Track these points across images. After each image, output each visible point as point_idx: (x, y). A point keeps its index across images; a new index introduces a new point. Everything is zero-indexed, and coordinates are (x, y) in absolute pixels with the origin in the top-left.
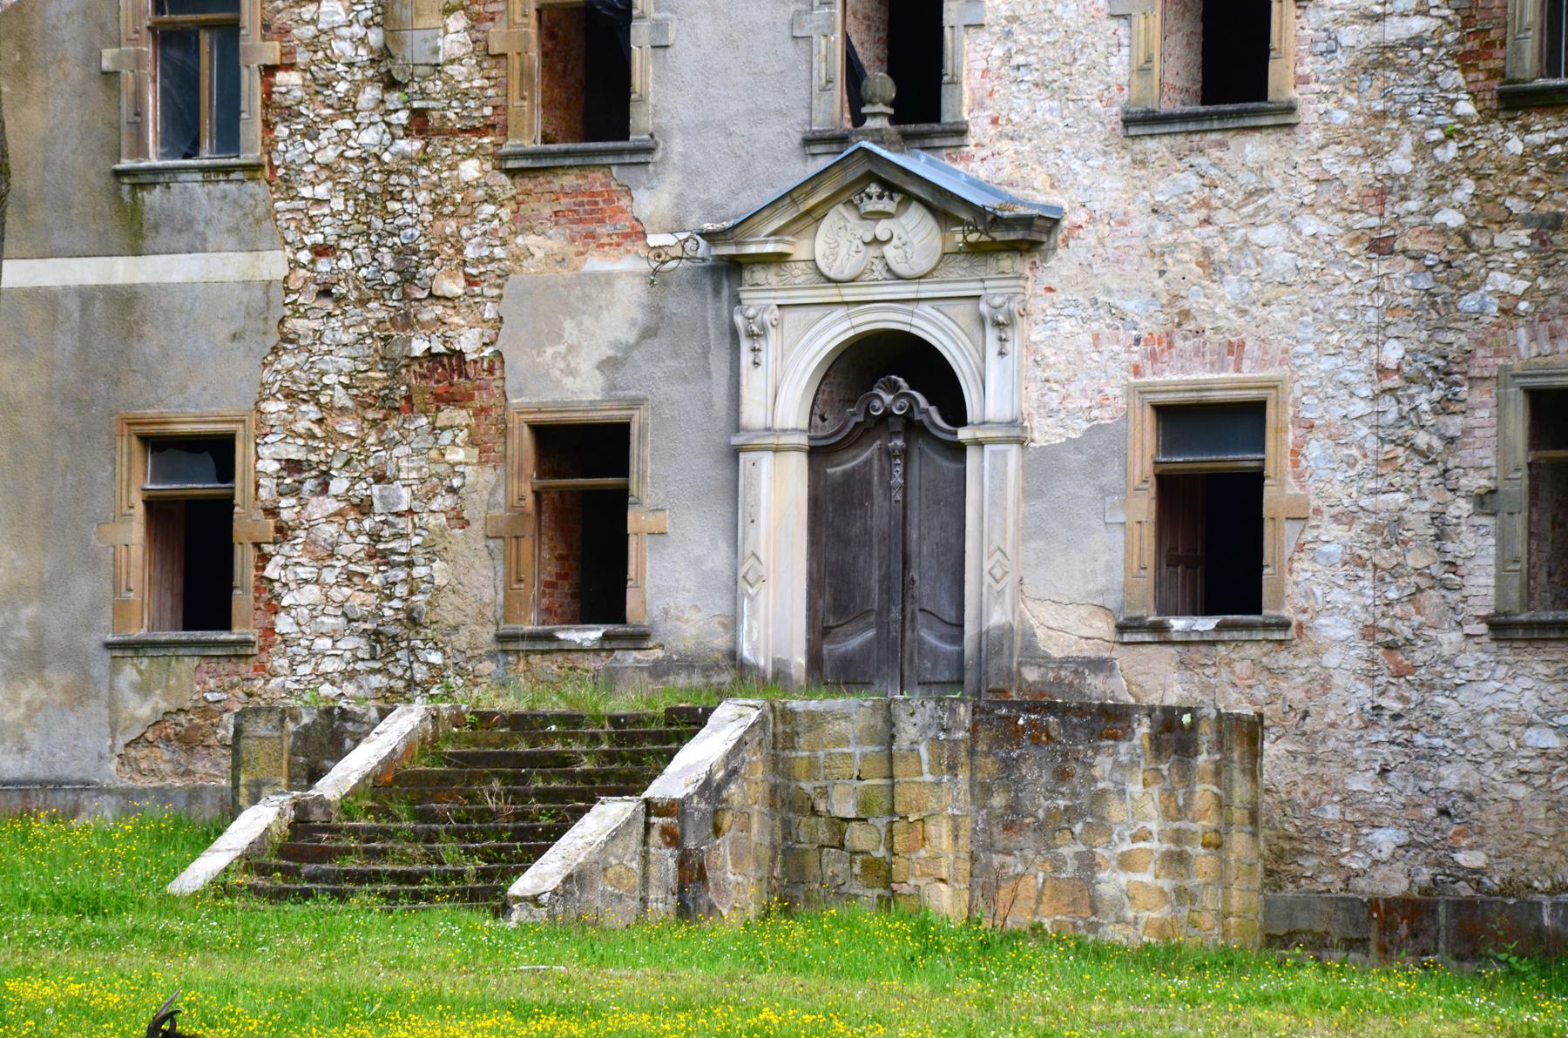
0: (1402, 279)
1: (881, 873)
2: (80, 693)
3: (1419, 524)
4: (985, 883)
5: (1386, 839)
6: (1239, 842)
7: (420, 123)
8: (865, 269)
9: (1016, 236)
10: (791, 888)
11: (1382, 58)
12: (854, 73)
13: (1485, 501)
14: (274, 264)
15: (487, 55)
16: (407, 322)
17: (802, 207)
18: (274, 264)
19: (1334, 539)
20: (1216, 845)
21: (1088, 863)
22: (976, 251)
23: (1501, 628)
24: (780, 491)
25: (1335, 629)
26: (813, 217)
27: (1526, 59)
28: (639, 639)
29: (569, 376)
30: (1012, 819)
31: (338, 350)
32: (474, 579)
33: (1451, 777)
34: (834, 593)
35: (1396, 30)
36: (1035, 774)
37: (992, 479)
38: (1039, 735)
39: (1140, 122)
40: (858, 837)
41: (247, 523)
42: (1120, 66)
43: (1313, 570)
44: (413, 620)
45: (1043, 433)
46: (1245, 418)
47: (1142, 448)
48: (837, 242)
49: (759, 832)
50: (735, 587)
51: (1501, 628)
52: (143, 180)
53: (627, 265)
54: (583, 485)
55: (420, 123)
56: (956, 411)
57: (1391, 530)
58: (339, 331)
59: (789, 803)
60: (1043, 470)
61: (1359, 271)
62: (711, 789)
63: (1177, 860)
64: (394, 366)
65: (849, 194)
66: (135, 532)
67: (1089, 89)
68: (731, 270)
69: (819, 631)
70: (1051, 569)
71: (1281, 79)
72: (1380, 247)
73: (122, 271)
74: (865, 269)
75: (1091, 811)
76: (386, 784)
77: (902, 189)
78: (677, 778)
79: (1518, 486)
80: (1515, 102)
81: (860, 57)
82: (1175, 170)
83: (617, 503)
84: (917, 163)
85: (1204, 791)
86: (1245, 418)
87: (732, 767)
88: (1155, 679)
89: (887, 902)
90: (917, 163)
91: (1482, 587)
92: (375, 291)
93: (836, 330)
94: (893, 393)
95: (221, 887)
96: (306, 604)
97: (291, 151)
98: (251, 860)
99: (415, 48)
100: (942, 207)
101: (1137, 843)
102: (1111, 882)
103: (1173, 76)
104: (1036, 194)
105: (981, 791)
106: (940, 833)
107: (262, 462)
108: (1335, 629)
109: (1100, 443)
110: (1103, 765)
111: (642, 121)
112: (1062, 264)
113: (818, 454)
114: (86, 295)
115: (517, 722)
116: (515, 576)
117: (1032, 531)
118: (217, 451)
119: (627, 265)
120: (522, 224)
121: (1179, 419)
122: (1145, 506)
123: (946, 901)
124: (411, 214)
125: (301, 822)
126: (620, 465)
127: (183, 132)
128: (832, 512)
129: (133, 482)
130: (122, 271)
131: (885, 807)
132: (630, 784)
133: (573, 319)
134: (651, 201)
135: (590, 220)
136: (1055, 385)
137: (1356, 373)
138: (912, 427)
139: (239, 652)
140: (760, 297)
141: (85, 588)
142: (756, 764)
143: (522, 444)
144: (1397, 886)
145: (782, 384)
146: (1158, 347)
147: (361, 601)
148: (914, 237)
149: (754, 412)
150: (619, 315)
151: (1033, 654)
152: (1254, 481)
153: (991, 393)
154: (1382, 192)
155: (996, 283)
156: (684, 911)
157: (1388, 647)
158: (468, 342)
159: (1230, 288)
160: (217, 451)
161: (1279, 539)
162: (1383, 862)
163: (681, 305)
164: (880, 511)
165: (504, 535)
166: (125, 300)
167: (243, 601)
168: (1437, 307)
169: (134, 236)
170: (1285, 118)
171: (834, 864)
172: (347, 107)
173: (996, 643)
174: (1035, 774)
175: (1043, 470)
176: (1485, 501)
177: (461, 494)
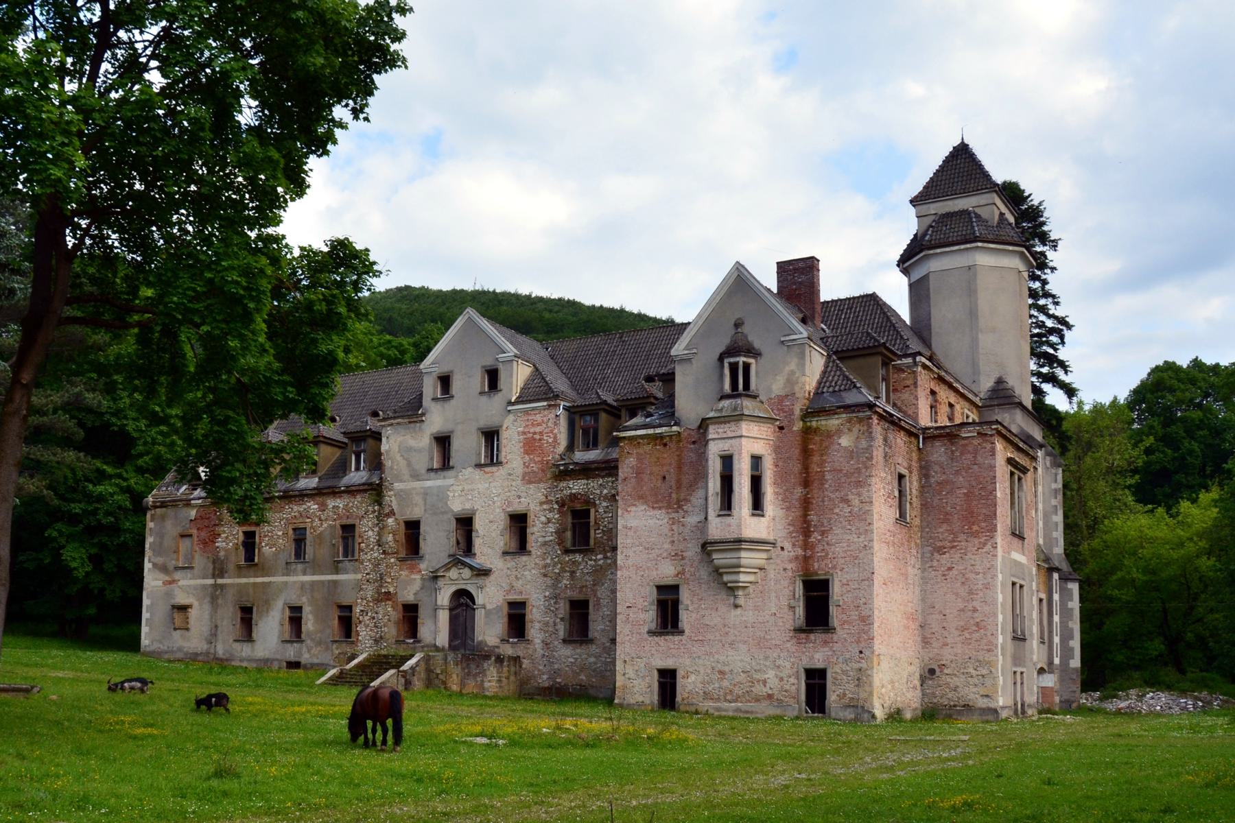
0: (549, 581)
1: (444, 683)
2: (327, 649)
3: (551, 623)
4: (463, 684)
5: (545, 677)
6: (512, 678)
7: (384, 552)
8: (458, 578)
9: (484, 573)
10: (429, 683)
11: (545, 544)
12: (458, 543)
13: (562, 619)
14: (359, 576)
15: (395, 540)
16: (381, 586)
17: (447, 567)
18: (359, 576)
19: (537, 625)
20: (508, 678)
21: (482, 681)
22: (478, 575)
23: (564, 641)
24: (444, 617)
25: (537, 641)
26: (449, 569)
27: (569, 544)
28: (419, 642)
29: (409, 596)
30: (469, 674)
31: (370, 591)
32: (391, 631)
33: (556, 666)
34: (453, 634)
35: (547, 539)
36: (473, 666)
37: (480, 615)
38: (473, 659)
39: (505, 553)
40: (441, 677)
41: (354, 620)
42: (502, 543)
43: (535, 632)
44: (381, 637)
45: (489, 607)
46: (523, 604)
47: (505, 610)
48: (453, 573)
49: (423, 675)
50: (436, 633)
51: (564, 641)
52: (339, 562)
53: (418, 577)
54: (410, 614)
55: (384, 552)
56: (474, 603)
57: (547, 624)
58: (370, 588)
59: (429, 671)
60: (488, 613)
61: (541, 580)
62: (412, 668)
63: (499, 681)
64: (379, 593)
65: (455, 565)
66: (336, 622)
67: (497, 548)
68: (436, 578)
69: (451, 641)
70: (489, 630)
71: (529, 547)
72: (545, 576)
73: (334, 577)
74: (458, 578)
75: (484, 672)
76: (360, 666)
77: (465, 564)
78: (407, 666)
79: (568, 616)
80: (567, 551)
81: (77, 326)
82: (511, 562)
83: (416, 618)
84: (467, 560)
85: (505, 669)
86: (523, 604)
87: (417, 664)
88: (508, 650)
89: (445, 688)
90: (467, 560)
91: (561, 634)
92: (376, 581)
93: (454, 588)
94: (463, 601)
95: (324, 683)
96: (364, 633)
97: (363, 557)
98: (330, 679)
99: (384, 540)
100: (471, 568)
101: (492, 678)
102: (487, 685)
103: (514, 545)
104: (488, 565)
105: (463, 669)
106: (454, 676)
107: (357, 610)
108: (537, 641)
109: (498, 609)
110: (485, 665)
111: (421, 552)
112: (492, 577)
113: (451, 610)
114: (329, 581)
115: (385, 656)
116: (398, 631)
117: (486, 624)
118: (349, 608)
119: (418, 577)
120: (401, 569)
121: (512, 604)
122: (506, 620)
123: (455, 688)
124: (383, 567)
125: (342, 672)
126: (417, 611)
127: (346, 554)
128: (453, 620)
129: (335, 614)
130: (334, 577)
131: (444, 671)
132: (397, 667)
133: (409, 587)
134: (423, 566)
135: (412, 569)
136: (490, 598)
137: (541, 597)
138: (467, 606)
139: (353, 643)
140: (441, 583)
141: (328, 631)
142: (423, 664)
143: (400, 607)
144: (547, 685)
145: (444, 598)
146: (508, 592)
147: (373, 634)
148: (467, 573)
149: (439, 603)
150: (416, 586)
151: (486, 645)
152: (524, 615)
153: (480, 600)
154: (545, 566)
155: (480, 581)
156: (199, 703)
157: (546, 644)
158: (391, 590)
159: (520, 582)
160: (349, 608)
161: (528, 625)
162: (544, 680)
163: (427, 584)
164: (462, 619)
165: (397, 623)
166: (335, 582)
167: (353, 634)
168: (554, 586)
169: (337, 572)
170: (529, 553)
171: (436, 681)
172: (372, 549)
173: (480, 643)
174: (473, 666)
175: (488, 613)
176: (562, 619)
177: (389, 614)
